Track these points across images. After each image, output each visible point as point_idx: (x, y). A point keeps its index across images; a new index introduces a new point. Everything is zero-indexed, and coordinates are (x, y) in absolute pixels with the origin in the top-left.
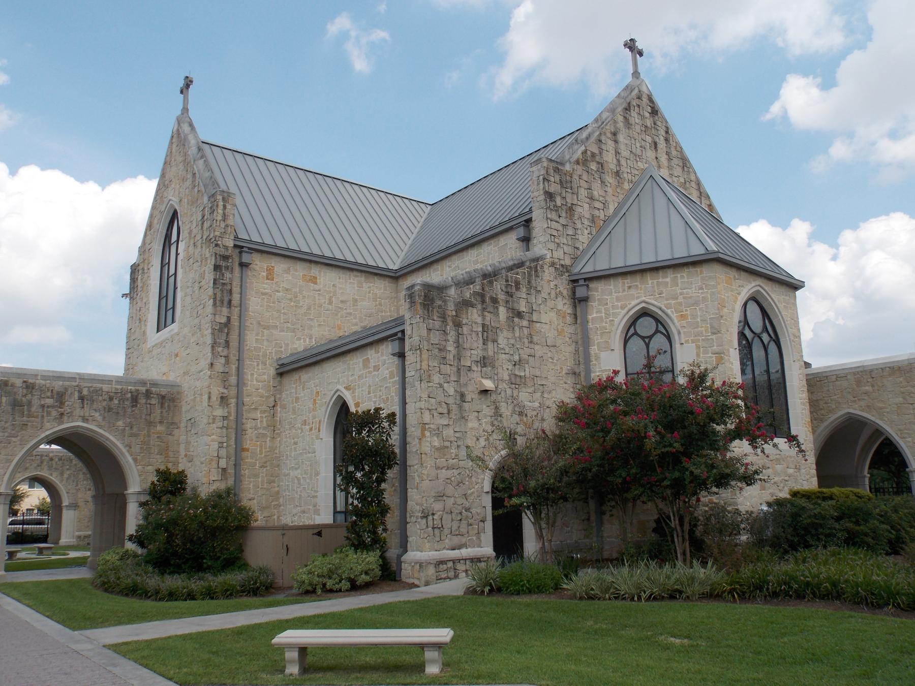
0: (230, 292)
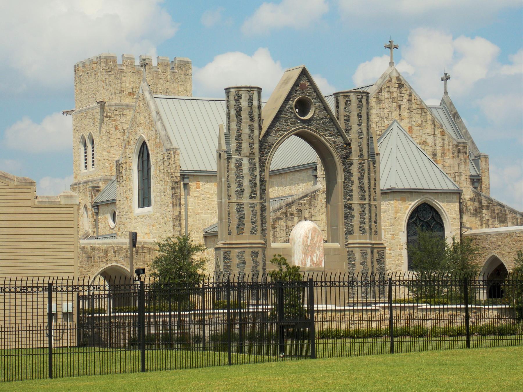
0: (180, 199)
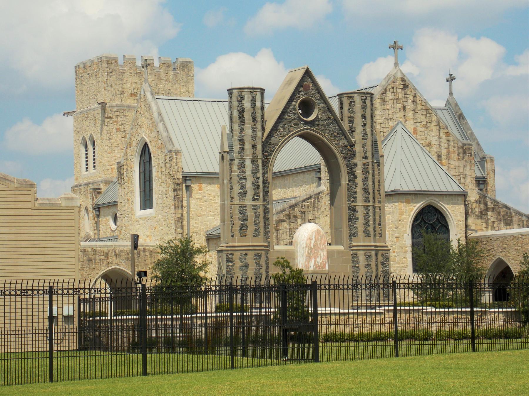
0: (182, 201)
